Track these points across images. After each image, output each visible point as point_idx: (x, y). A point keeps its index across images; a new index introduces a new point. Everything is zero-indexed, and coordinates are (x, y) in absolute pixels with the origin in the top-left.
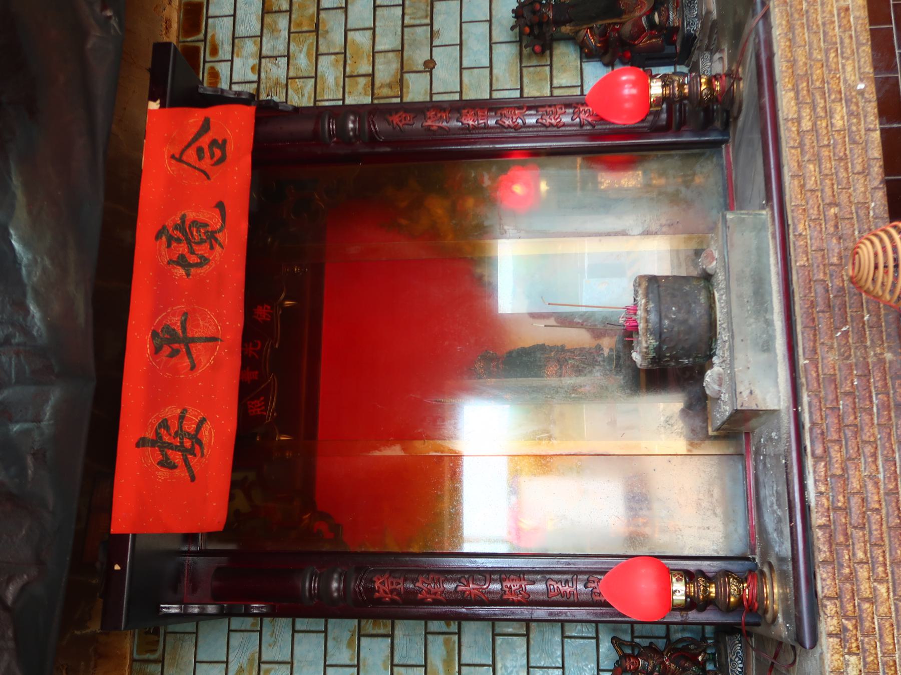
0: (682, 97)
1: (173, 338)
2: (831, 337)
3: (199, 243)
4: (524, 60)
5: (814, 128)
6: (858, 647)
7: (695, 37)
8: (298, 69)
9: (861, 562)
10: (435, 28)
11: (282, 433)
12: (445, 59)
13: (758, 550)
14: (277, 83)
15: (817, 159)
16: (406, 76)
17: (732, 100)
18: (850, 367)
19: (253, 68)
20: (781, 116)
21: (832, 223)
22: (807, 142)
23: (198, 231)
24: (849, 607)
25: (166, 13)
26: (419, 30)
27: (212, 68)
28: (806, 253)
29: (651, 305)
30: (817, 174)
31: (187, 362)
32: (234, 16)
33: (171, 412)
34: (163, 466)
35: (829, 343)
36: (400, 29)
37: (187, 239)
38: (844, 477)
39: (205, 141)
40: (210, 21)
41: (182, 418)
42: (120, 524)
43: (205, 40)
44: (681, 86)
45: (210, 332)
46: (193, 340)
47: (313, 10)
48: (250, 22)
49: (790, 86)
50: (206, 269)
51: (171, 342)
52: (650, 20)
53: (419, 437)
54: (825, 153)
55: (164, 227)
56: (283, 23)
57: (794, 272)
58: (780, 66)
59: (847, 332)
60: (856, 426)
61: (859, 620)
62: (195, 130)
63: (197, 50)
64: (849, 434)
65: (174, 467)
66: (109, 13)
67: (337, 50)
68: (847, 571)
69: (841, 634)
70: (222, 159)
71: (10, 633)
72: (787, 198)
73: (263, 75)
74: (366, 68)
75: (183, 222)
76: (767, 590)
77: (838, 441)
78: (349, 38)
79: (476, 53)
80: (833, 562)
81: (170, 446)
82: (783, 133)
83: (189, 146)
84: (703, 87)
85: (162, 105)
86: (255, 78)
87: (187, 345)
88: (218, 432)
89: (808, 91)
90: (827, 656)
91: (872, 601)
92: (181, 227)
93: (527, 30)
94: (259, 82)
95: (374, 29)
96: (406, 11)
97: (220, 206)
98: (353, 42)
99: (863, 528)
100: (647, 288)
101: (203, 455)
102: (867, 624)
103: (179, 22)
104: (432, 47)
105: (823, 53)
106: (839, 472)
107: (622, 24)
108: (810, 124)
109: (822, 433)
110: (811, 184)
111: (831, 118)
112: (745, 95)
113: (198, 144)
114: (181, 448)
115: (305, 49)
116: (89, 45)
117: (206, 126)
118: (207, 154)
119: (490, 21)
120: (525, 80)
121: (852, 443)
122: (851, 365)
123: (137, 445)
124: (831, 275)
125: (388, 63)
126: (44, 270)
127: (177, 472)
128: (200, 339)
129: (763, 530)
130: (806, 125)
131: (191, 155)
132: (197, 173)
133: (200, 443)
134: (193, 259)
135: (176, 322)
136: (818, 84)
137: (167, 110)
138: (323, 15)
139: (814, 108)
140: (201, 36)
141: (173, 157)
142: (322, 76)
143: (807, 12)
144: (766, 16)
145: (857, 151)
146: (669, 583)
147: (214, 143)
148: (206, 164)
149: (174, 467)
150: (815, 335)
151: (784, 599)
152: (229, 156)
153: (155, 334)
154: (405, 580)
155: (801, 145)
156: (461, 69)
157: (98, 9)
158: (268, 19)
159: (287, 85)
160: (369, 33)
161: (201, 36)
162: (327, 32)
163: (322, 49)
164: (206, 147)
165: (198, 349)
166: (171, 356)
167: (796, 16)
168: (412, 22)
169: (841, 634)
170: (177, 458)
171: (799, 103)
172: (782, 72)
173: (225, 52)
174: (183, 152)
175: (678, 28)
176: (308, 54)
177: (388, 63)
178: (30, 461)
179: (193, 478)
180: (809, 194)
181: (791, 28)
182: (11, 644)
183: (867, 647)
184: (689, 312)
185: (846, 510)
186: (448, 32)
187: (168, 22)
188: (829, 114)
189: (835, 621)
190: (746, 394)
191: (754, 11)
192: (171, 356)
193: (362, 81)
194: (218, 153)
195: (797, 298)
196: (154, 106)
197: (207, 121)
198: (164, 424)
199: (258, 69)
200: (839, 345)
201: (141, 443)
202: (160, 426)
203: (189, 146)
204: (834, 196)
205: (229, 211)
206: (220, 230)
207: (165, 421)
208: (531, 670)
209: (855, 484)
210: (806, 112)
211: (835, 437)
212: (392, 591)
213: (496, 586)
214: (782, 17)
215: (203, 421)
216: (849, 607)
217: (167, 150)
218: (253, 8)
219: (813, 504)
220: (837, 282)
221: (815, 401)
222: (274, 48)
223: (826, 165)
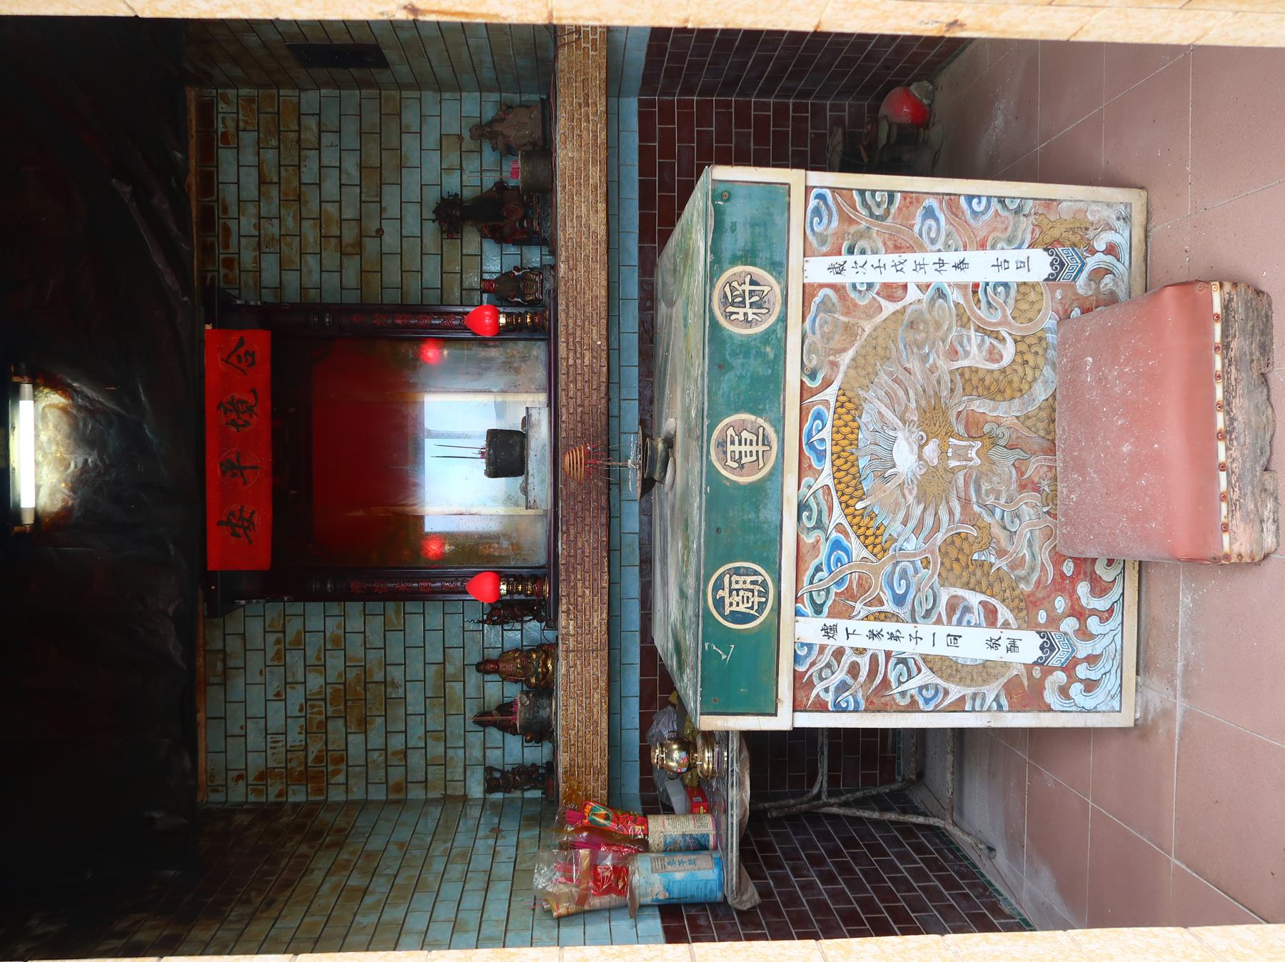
12: (390, 229)
14: (273, 239)
39: (241, 351)
41: (241, 510)
42: (212, 565)
47: (296, 183)
48: (251, 190)
56: (274, 192)
58: (561, 328)
63: (212, 208)
69: (568, 612)
79: (412, 226)
80: (568, 580)
85: (214, 327)
88: (261, 519)
91: (583, 596)
94: (259, 236)
95: (340, 202)
97: (253, 391)
110: (571, 394)
117: (241, 343)
129: (556, 555)
130: (571, 362)
131: (234, 358)
134: (240, 422)
138: (303, 188)
140: (214, 198)
145: (595, 377)
147: (246, 352)
155: (568, 373)
158: (264, 188)
161: (214, 198)
169: (568, 612)
171: (568, 349)
181: (567, 306)
185: (575, 556)
186: (393, 211)
188: (583, 357)
193: (333, 241)
196: (208, 327)
209: (580, 545)
210: (571, 354)
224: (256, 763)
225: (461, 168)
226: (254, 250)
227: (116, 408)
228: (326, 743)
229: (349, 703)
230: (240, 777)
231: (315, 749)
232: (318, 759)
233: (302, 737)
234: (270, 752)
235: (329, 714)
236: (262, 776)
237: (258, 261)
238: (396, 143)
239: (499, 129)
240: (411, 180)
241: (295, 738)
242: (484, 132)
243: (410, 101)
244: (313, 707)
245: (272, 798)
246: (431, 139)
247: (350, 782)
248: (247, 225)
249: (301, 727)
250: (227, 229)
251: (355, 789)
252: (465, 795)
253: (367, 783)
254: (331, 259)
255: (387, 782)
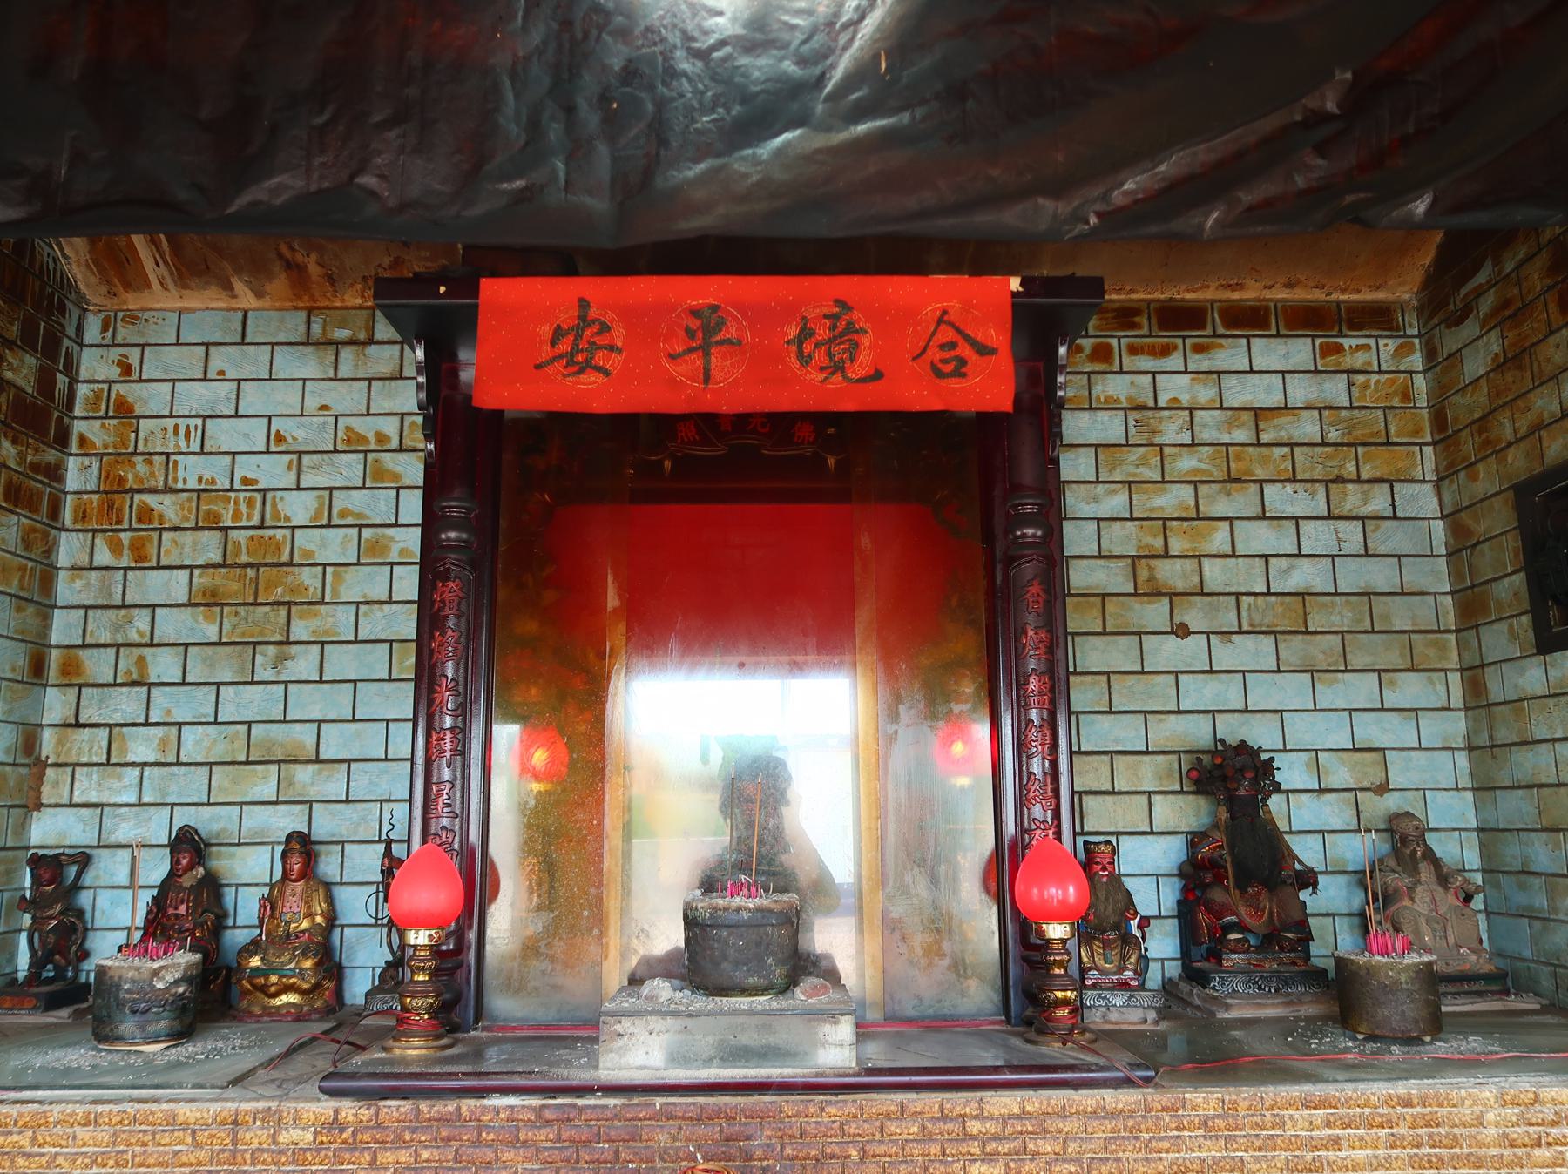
0: (1048, 966)
1: (709, 330)
2: (688, 1140)
3: (829, 352)
4: (1189, 756)
5: (968, 1137)
6: (322, 1143)
7: (1204, 987)
8: (1174, 458)
9: (417, 1155)
10: (1235, 637)
11: (837, 462)
12: (1190, 651)
13: (484, 1034)
15: (926, 1137)
16: (1166, 600)
17: (1042, 1031)
18: (650, 1160)
19: (1175, 400)
20: (987, 1095)
21: (837, 1152)
22: (949, 1126)
23: (845, 350)
24: (367, 1137)
25: (1250, 283)
26: (1233, 616)
27: (1175, 348)
28: (797, 1115)
29: (746, 915)
30: (904, 1136)
31: (679, 349)
32: (1252, 371)
33: (619, 336)
34: (555, 331)
35: (681, 1136)
36: (1233, 590)
37: (835, 338)
38: (515, 1142)
39: (965, 351)
40: (1244, 341)
41: (611, 348)
43: (1215, 336)
44: (1062, 964)
45: (716, 374)
46: (707, 354)
47: (1261, 474)
48: (1241, 393)
49: (1028, 1108)
50: (793, 361)
51: (705, 329)
52: (1230, 928)
53: (629, 629)
54: (935, 1149)
55: (850, 308)
56: (1241, 435)
57: (774, 1098)
58: (1056, 1097)
59: (695, 1159)
60: (577, 1162)
61: (351, 1146)
62: (980, 337)
64: (567, 1153)
65: (553, 344)
66: (1093, 220)
67: (1202, 508)
68: (408, 1138)
70: (938, 373)
71: (326, 185)
72: (874, 1096)
73: (1166, 413)
74: (1176, 546)
75: (857, 332)
76: (416, 1042)
77: (559, 1139)
78: (1220, 523)
79: (1198, 692)
80: (417, 1122)
81: (578, 337)
82: (963, 1096)
83: (958, 330)
84: (1060, 994)
85: (1015, 295)
86: (1161, 403)
87: (700, 347)
88: (594, 391)
89: (1021, 1133)
90: (314, 1107)
92: (851, 329)
93: (1219, 761)
94: (1156, 408)
95: (1234, 555)
96: (1260, 600)
97: (877, 375)
98: (1214, 529)
99: (456, 1160)
100: (771, 911)
101: (565, 376)
102: (347, 1156)
103: (1241, 300)
104: (1208, 633)
105: (1074, 1156)
106: (522, 1137)
107: (1227, 889)
108: (975, 1132)
109: (569, 1120)
110: (892, 1127)
111: (983, 1161)
112: (1043, 1049)
113: (961, 342)
114: (575, 350)
115: (1203, 466)
116: (1041, 201)
117: (984, 350)
118: (946, 355)
119: (1246, 711)
120: (1160, 758)
121: (556, 1155)
122: (652, 1161)
123: (581, 300)
124: (768, 1145)
125: (1184, 576)
126: (746, 176)
127: (547, 348)
128: (709, 362)
130: (974, 1127)
132: (922, 344)
133: (581, 371)
134: (808, 347)
135: (732, 333)
136: (1031, 1146)
137: (1009, 299)
138: (1254, 488)
139: (996, 1138)
140: (1221, 330)
141: (945, 312)
142: (1165, 491)
143: (1136, 1138)
144: (1128, 1082)
146: (427, 926)
147: (963, 362)
148: (934, 354)
149: (553, 344)
150: (691, 1119)
151: (404, 1061)
152: (944, 382)
153: (714, 309)
154: (458, 617)
155: (945, 1118)
156: (1177, 673)
157: (1099, 207)
158: (1247, 417)
159: (1152, 445)
160: (1228, 549)
161: (1221, 330)
162: (1229, 494)
163: (1203, 489)
164: (958, 352)
165: (697, 360)
166: (687, 330)
167: (1130, 1123)
168: (1244, 607)
169: (336, 1124)
170: (564, 347)
171: (1005, 1119)
172: (1049, 1099)
173: (1199, 362)
174: (951, 324)
175: (1221, 965)
176: (1196, 471)
177: (1184, 576)
178: (519, 184)
179: (538, 367)
180: (878, 1124)
181: (1112, 1115)
182: (314, 187)
183: (323, 1154)
184: (737, 963)
185: (478, 1142)
186: (1225, 656)
187: (1239, 287)
189: (350, 1118)
190: (619, 1028)
191: (1138, 1066)
192: (687, 330)
193: (1158, 543)
194: (949, 368)
195: (740, 1099)
196: (1015, 284)
197: (993, 351)
198: (605, 328)
199: (1174, 406)
200: (679, 1148)
201: (583, 304)
202: (602, 324)
203: (958, 330)
204: (874, 1156)
205: (871, 386)
206: (845, 378)
207: (608, 329)
208: (345, 766)
209: (507, 1155)
210: (992, 1128)
211: (565, 1135)
212: (443, 601)
213: (448, 722)
214: (1127, 1103)
215: (606, 373)
216: (367, 1137)
217: (954, 305)
218: (1263, 396)
219: (486, 1102)
220: (758, 1153)
221: (609, 1114)
222: (1205, 426)
223: (916, 1149)
224: (150, 398)
225: (1321, 791)
226: (1129, 399)
227: (838, 74)
228: (176, 529)
229: (250, 572)
230: (127, 370)
231: (167, 507)
232: (146, 514)
233: (193, 484)
234: (170, 423)
235: (233, 534)
236: (124, 410)
237: (1110, 406)
238: (1356, 661)
239: (1424, 877)
240: (1291, 691)
241: (191, 471)
242: (1405, 842)
243: (1441, 689)
244: (250, 503)
245: (79, 427)
246: (1373, 730)
247: (94, 573)
248: (1176, 387)
249: (213, 482)
250: (1165, 351)
251: (78, 584)
252: (39, 806)
253: (87, 608)
254: (1123, 539)
255: (84, 646)
